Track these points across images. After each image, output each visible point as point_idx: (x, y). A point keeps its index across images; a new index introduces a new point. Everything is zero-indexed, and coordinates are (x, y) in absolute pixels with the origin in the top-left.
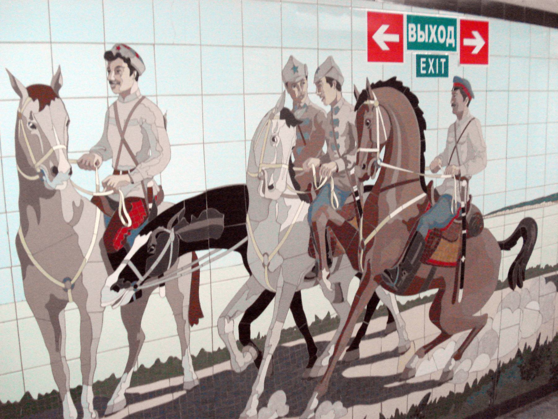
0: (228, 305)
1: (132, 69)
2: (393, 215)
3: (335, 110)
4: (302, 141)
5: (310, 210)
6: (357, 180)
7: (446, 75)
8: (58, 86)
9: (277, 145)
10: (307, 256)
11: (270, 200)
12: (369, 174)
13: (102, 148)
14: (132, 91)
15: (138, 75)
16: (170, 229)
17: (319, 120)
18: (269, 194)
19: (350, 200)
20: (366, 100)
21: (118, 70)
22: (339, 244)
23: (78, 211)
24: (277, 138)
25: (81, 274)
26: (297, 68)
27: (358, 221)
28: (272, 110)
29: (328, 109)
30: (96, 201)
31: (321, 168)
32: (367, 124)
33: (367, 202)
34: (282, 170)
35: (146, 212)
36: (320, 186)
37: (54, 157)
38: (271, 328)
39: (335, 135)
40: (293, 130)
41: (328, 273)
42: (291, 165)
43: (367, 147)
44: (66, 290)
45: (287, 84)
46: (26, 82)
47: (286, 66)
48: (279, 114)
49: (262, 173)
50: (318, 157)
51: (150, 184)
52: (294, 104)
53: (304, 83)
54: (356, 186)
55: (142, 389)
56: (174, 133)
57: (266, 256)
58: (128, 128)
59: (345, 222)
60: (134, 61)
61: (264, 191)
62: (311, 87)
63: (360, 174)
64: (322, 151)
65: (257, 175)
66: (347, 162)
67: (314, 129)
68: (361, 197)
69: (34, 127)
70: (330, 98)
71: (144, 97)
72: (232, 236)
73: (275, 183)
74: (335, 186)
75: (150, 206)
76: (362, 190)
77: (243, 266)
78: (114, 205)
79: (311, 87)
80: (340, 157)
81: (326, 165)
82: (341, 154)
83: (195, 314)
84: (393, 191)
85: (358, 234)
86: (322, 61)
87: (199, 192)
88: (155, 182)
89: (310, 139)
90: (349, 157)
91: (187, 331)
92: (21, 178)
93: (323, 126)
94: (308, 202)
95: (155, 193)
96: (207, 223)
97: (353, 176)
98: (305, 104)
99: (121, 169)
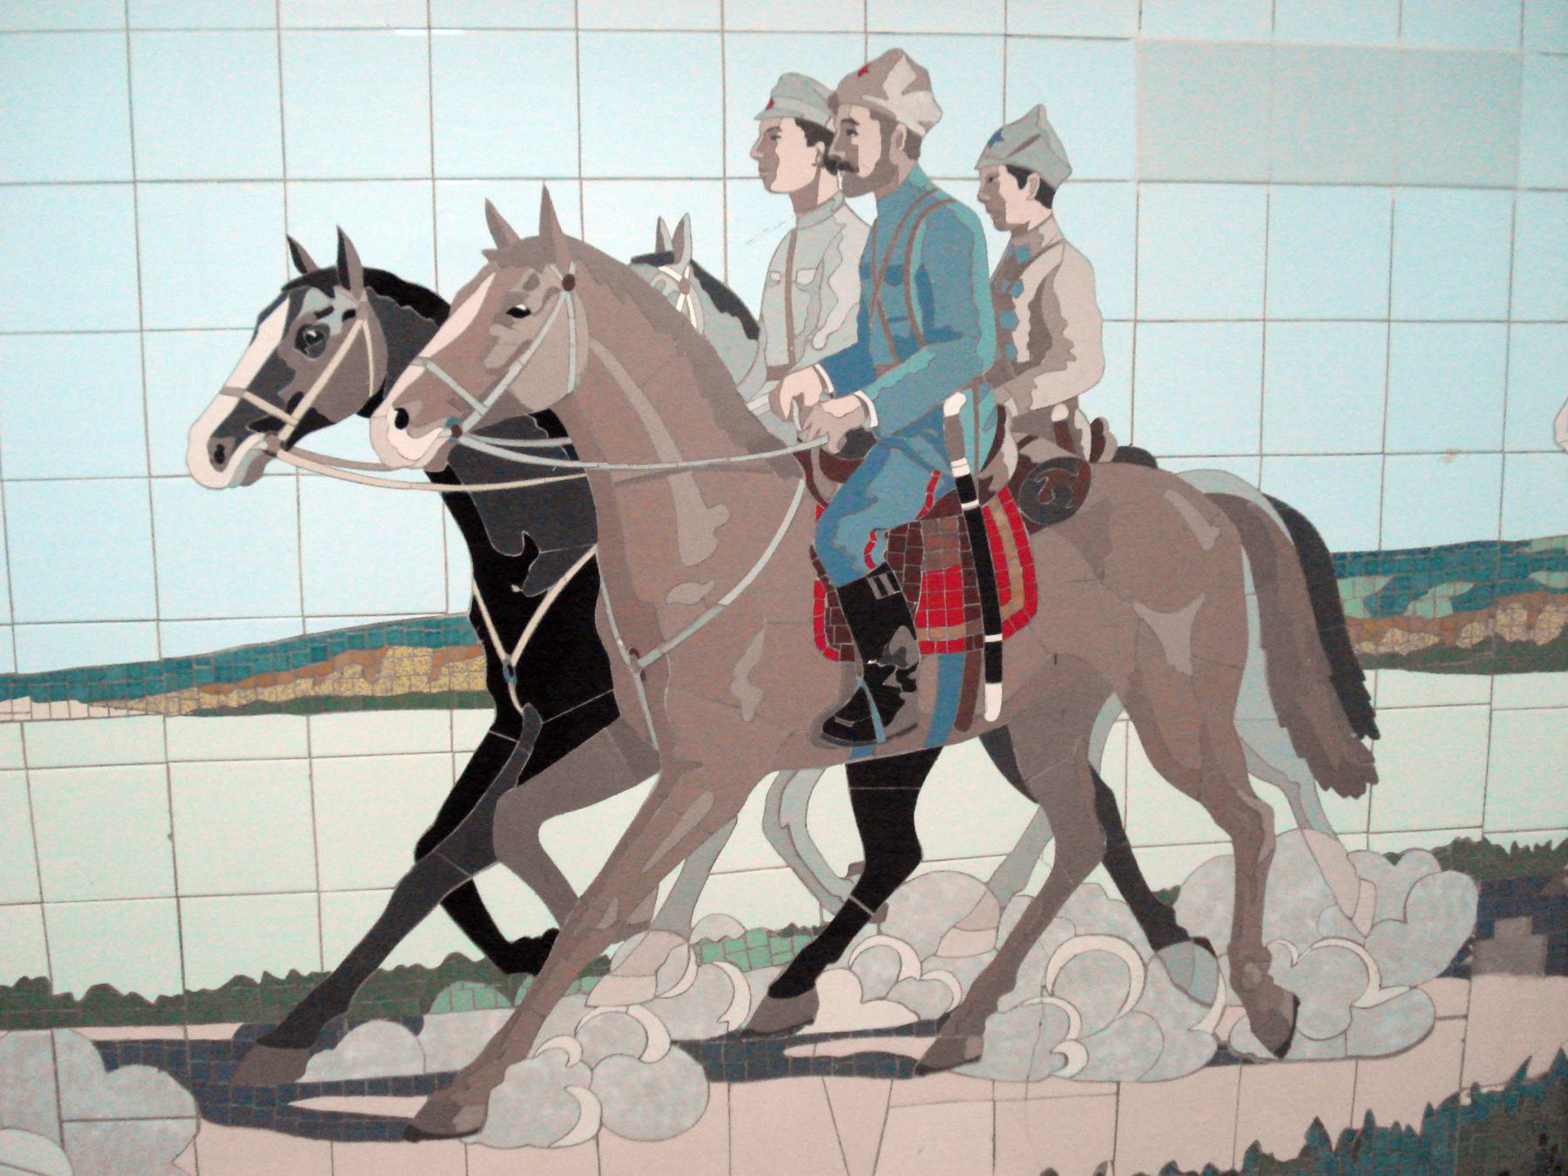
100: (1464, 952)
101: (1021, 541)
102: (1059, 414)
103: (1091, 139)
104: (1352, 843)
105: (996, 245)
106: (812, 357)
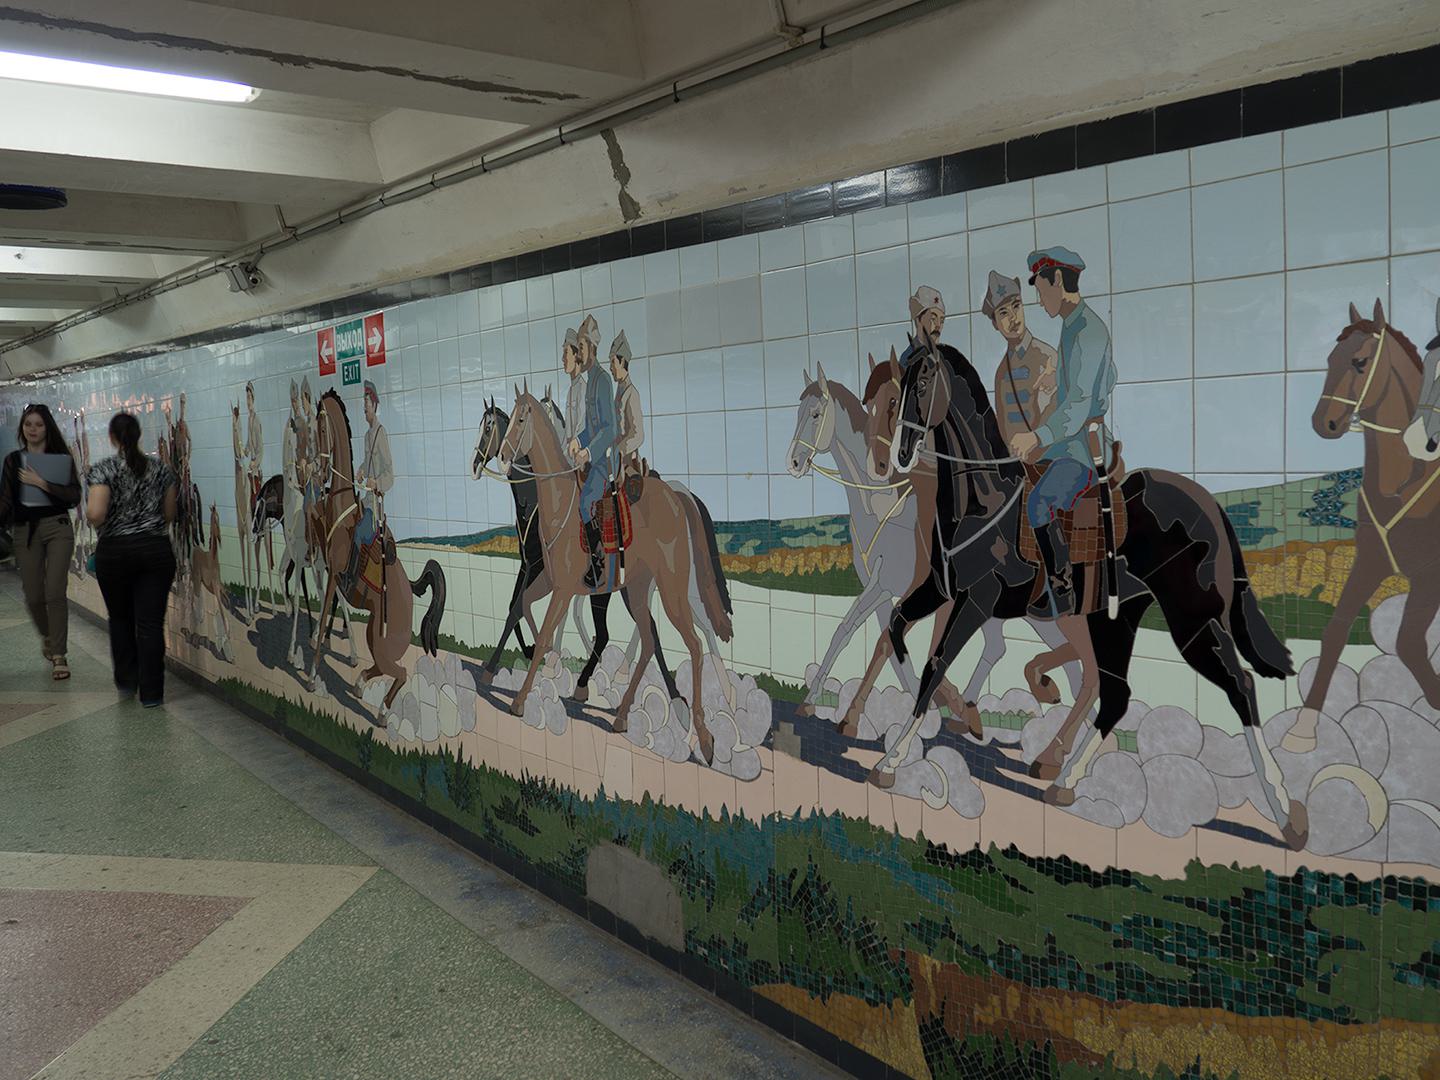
2: (340, 519)
7: (359, 381)
84: (339, 495)
100: (769, 735)
101: (628, 509)
102: (634, 457)
103: (637, 347)
104: (728, 665)
105: (615, 385)
106: (576, 435)
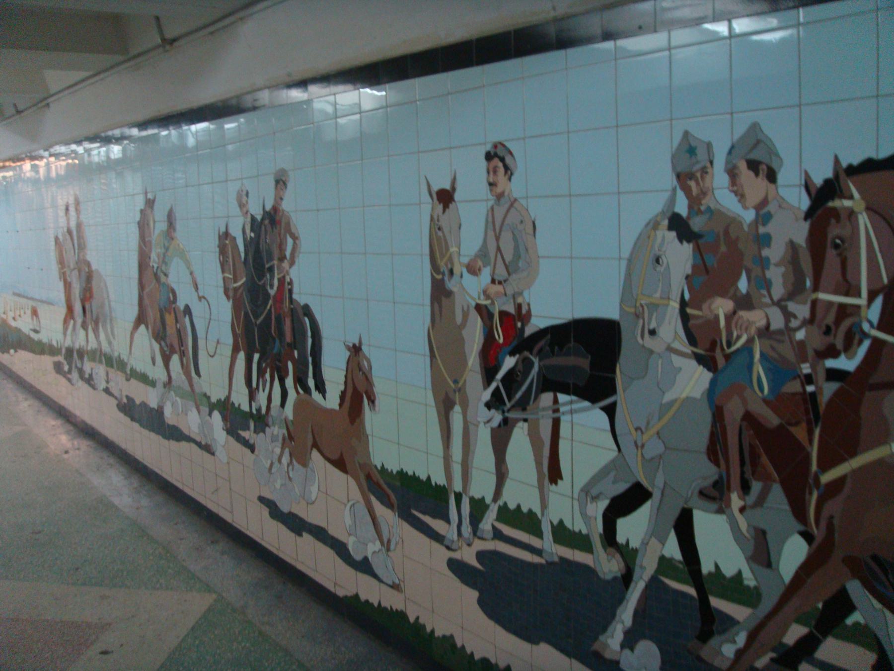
0: (463, 448)
1: (506, 168)
3: (764, 218)
4: (701, 267)
5: (713, 383)
6: (810, 353)
8: (454, 189)
9: (662, 270)
10: (704, 458)
11: (651, 352)
12: (839, 344)
13: (483, 254)
14: (506, 194)
15: (512, 174)
16: (535, 357)
17: (733, 235)
18: (648, 342)
19: (794, 387)
20: (833, 199)
21: (495, 172)
22: (764, 459)
23: (466, 315)
24: (664, 260)
25: (465, 381)
26: (696, 148)
27: (810, 433)
28: (657, 216)
29: (749, 216)
30: (478, 308)
31: (736, 317)
32: (836, 246)
33: (831, 401)
34: (669, 309)
35: (508, 331)
36: (733, 348)
37: (451, 259)
38: (645, 542)
39: (764, 263)
40: (687, 249)
41: (741, 503)
42: (683, 304)
43: (836, 292)
44: (455, 391)
45: (678, 176)
46: (435, 188)
47: (678, 149)
48: (666, 222)
49: (641, 309)
50: (731, 298)
51: (520, 300)
52: (690, 207)
53: (707, 173)
54: (808, 365)
55: (507, 530)
56: (543, 243)
57: (639, 433)
58: (503, 233)
59: (780, 427)
60: (508, 160)
61: (642, 337)
62: (719, 179)
63: (818, 342)
64: (737, 288)
65: (633, 310)
66: (788, 316)
67: (723, 248)
68: (820, 389)
69: (439, 229)
70: (754, 198)
71: (516, 200)
72: (598, 388)
73: (659, 326)
74: (762, 354)
75: (519, 325)
76: (821, 375)
77: (609, 436)
78: (491, 316)
79: (719, 179)
80: (774, 303)
81: (744, 314)
82: (776, 297)
83: (555, 474)
85: (808, 457)
86: (740, 130)
87: (558, 318)
88: (524, 298)
89: (716, 265)
90: (792, 306)
91: (546, 490)
92: (433, 277)
93: (741, 246)
94: (709, 370)
95: (524, 311)
96: (571, 361)
97: (801, 343)
98: (709, 208)
99: (497, 278)
